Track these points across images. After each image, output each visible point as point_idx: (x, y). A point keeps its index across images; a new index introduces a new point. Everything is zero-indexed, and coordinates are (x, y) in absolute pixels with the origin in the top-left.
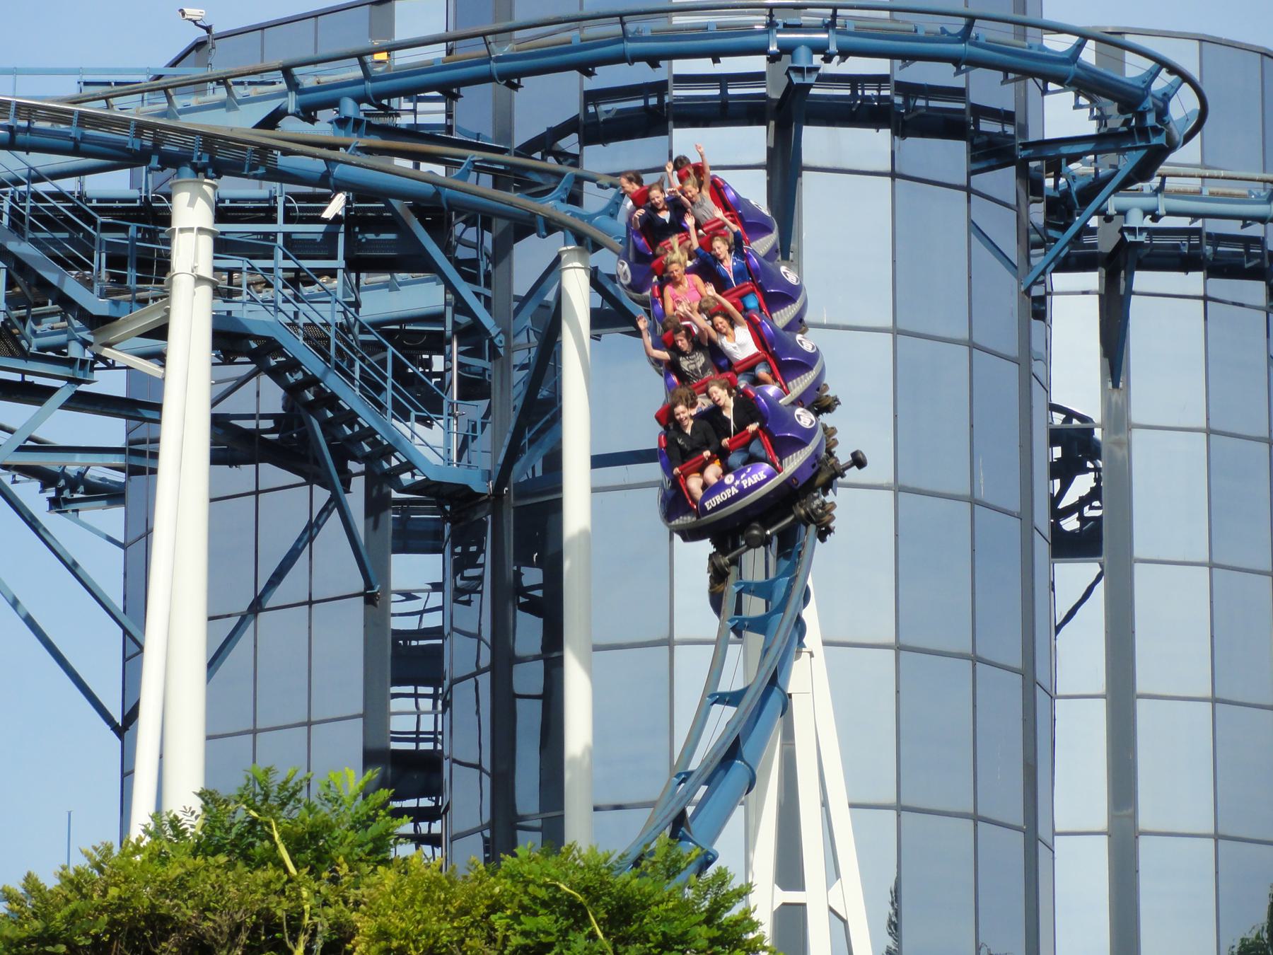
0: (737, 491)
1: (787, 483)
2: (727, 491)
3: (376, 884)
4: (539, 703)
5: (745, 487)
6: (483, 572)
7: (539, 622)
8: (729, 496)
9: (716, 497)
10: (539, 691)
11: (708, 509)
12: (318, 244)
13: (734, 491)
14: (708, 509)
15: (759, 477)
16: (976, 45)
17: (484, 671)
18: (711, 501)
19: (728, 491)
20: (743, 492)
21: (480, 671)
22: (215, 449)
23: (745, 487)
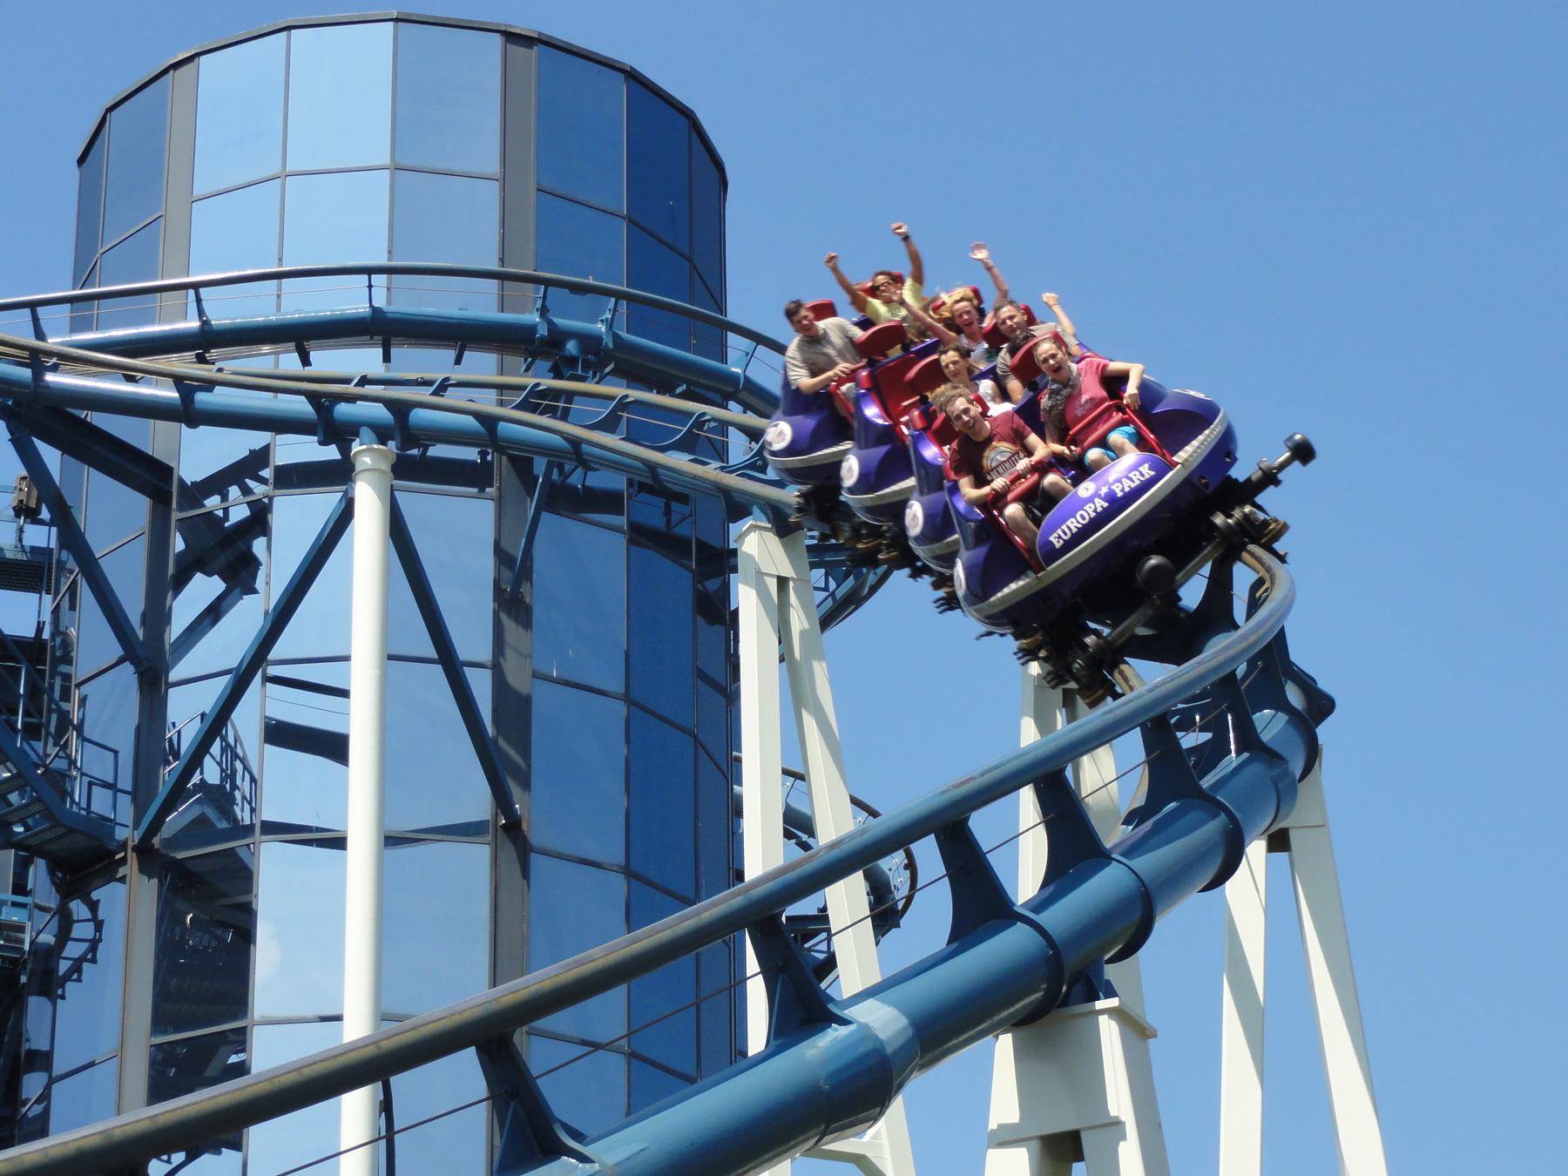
0: (1106, 505)
1: (1187, 484)
2: (1086, 508)
3: (996, 468)
4: (495, 186)
5: (1120, 494)
6: (126, 854)
7: (217, 387)
8: (1093, 515)
9: (1069, 523)
10: (366, 276)
11: (1058, 546)
12: (11, 761)
13: (1101, 504)
14: (1058, 546)
15: (1142, 475)
16: (951, 501)
17: (382, 1138)
18: (1059, 531)
19: (1090, 508)
20: (1116, 504)
21: (380, 1138)
22: (234, 1018)
23: (1120, 494)
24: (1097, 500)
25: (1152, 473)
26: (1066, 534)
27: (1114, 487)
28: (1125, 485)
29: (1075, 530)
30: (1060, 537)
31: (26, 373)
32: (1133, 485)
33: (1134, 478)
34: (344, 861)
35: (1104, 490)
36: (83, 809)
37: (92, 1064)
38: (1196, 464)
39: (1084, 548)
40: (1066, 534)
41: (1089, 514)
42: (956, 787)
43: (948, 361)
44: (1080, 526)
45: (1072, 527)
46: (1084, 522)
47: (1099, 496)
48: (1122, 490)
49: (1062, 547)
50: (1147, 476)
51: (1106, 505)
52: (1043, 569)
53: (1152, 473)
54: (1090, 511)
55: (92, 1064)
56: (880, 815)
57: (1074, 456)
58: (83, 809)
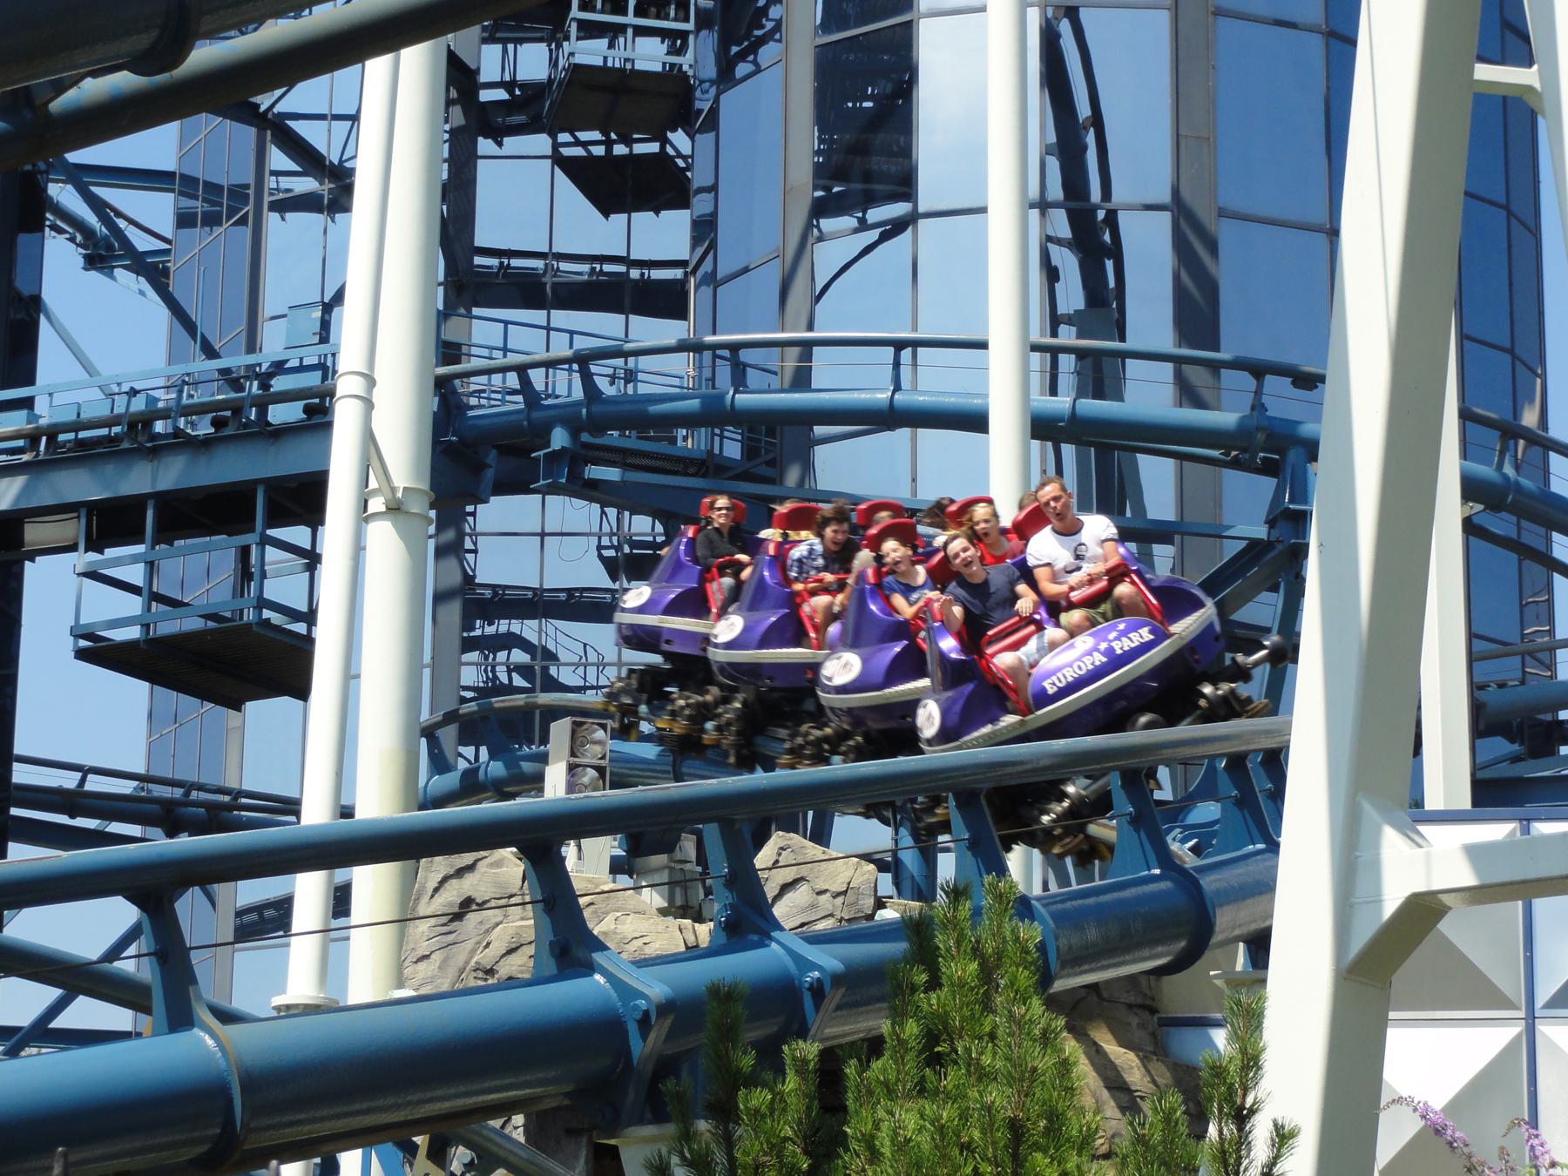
0: (1104, 659)
5: (1119, 652)
8: (1091, 667)
15: (1141, 637)
24: (1095, 654)
25: (1152, 637)
26: (1060, 681)
27: (1113, 644)
28: (1125, 644)
29: (1070, 679)
30: (1054, 684)
31: (651, 539)
32: (1133, 645)
33: (1134, 639)
34: (988, 441)
35: (1103, 646)
36: (717, 435)
37: (746, 270)
38: (1189, 638)
39: (1063, 705)
40: (1060, 681)
41: (1065, 677)
42: (71, 1049)
43: (1048, 497)
44: (1076, 676)
45: (1067, 675)
46: (1081, 673)
47: (1098, 650)
48: (1121, 648)
49: (1055, 694)
50: (1147, 639)
51: (1104, 659)
52: (1032, 713)
53: (1152, 637)
54: (1088, 663)
55: (746, 270)
56: (1450, 908)
57: (988, 662)
58: (717, 435)
